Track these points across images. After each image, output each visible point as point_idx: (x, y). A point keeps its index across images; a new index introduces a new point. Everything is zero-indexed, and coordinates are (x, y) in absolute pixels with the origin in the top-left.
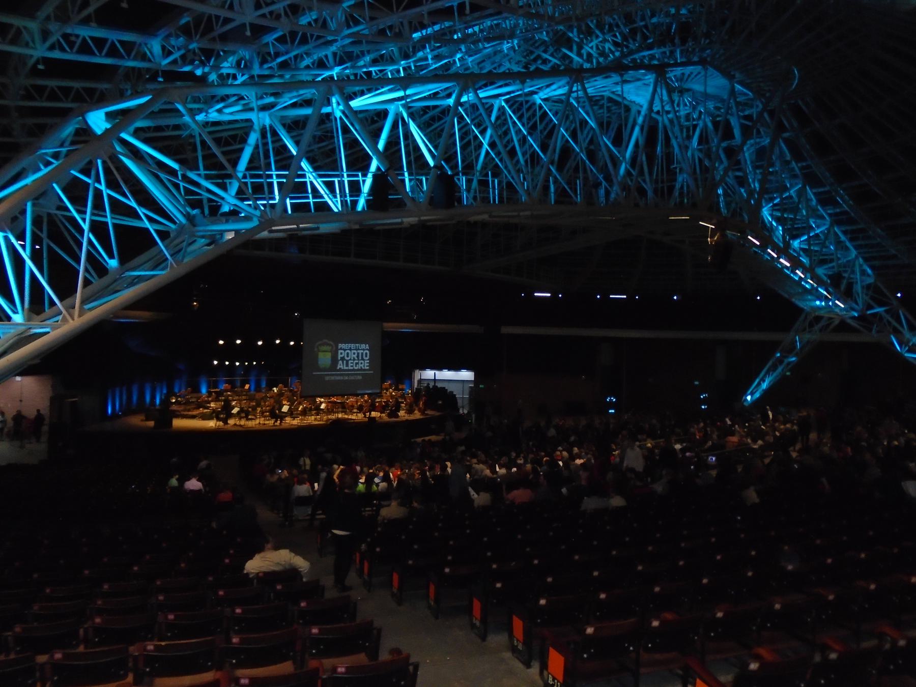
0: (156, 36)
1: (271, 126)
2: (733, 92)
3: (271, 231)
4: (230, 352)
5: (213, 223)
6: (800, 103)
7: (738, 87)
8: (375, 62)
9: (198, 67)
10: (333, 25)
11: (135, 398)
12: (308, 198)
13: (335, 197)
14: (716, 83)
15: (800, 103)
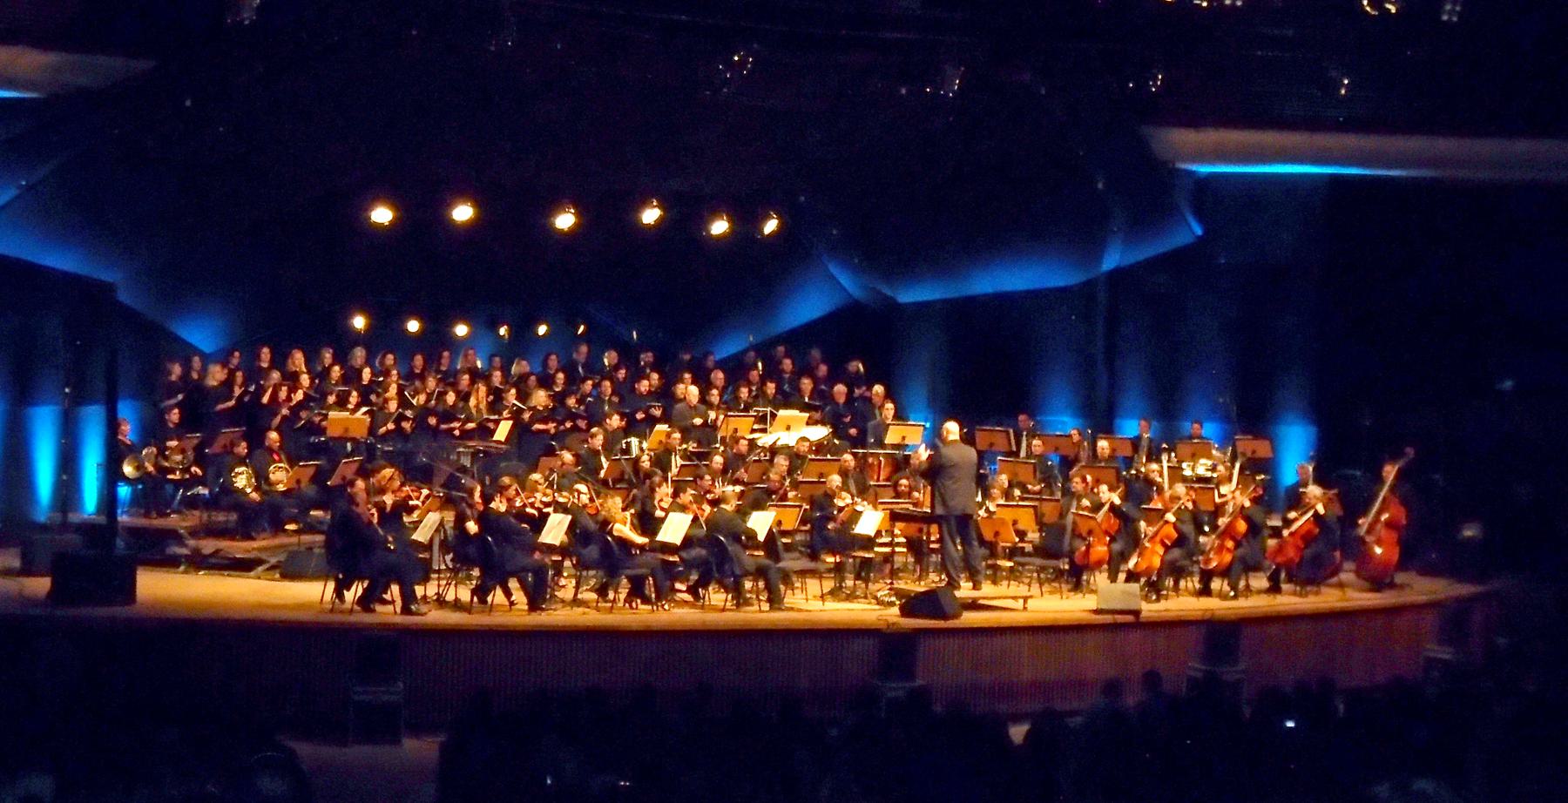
4: (428, 276)
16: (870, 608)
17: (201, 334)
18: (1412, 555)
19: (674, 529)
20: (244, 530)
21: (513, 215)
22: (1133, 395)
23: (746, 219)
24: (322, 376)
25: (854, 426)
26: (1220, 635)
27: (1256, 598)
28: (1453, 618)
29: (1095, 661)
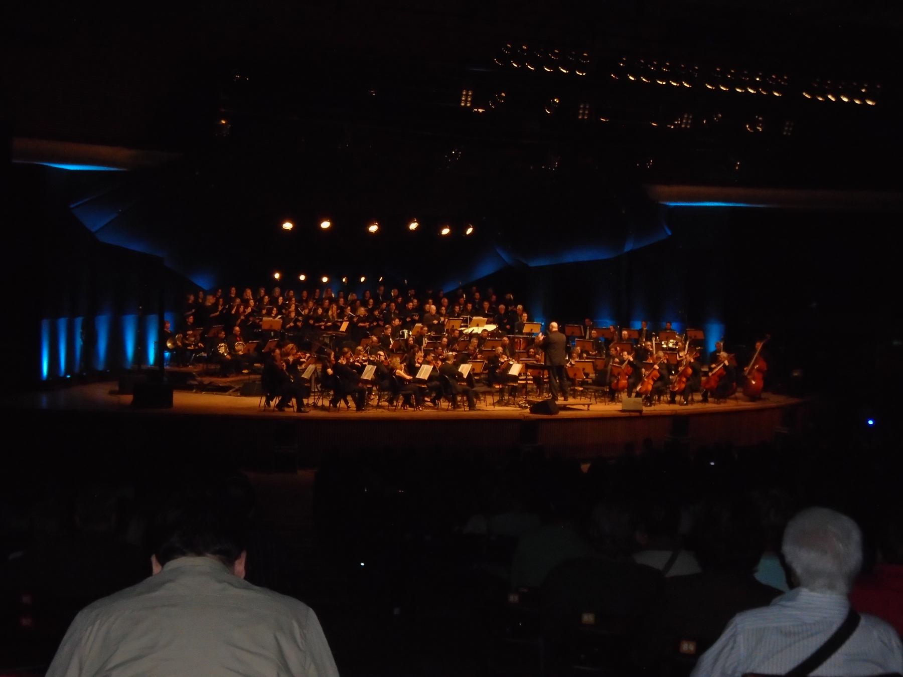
4: (307, 251)
21: (349, 226)
26: (677, 420)
27: (696, 405)
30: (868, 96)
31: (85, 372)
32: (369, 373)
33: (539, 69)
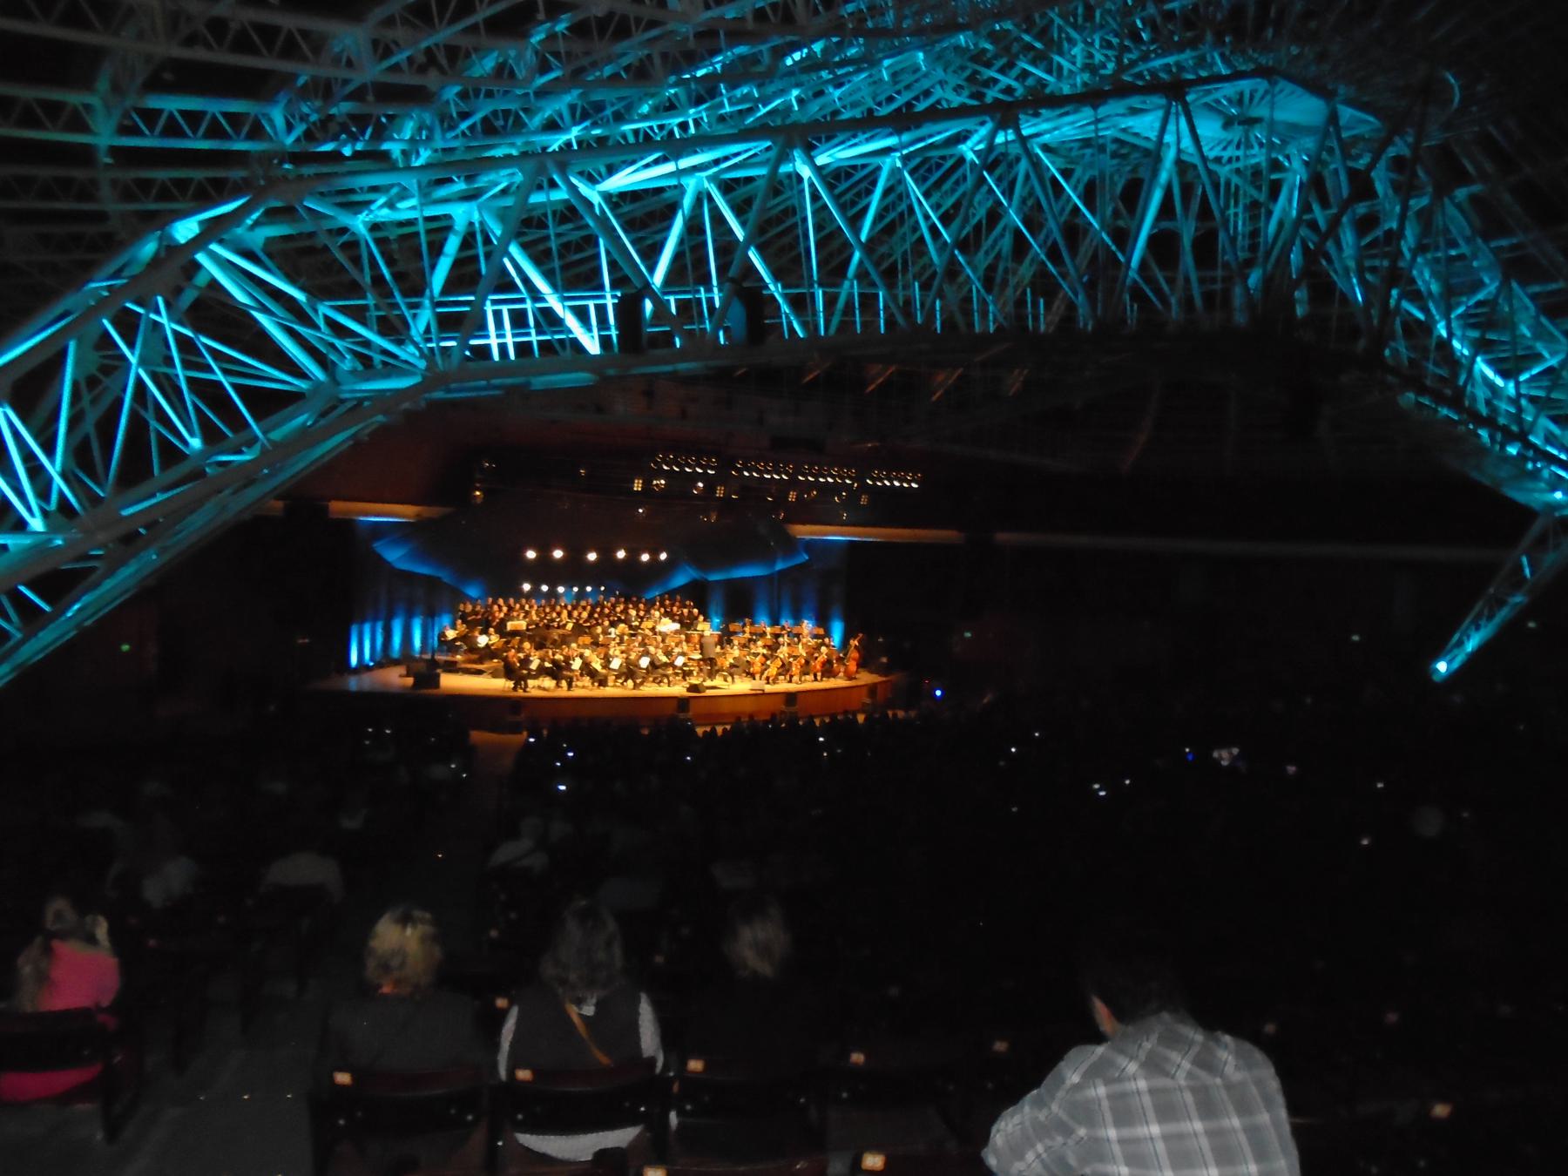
0: (277, 102)
1: (481, 223)
2: (1333, 118)
3: (449, 391)
4: (545, 571)
5: (367, 379)
6: (1491, 129)
7: (1346, 113)
8: (657, 111)
9: (344, 144)
10: (521, 73)
11: (397, 640)
12: (528, 334)
13: (590, 330)
14: (1299, 108)
15: (1491, 129)
16: (678, 689)
17: (473, 591)
18: (863, 664)
19: (616, 664)
20: (480, 661)
21: (575, 555)
22: (786, 612)
23: (654, 554)
24: (511, 609)
25: (687, 624)
26: (790, 697)
27: (809, 684)
28: (872, 689)
29: (748, 707)
30: (913, 480)
31: (385, 660)
32: (577, 664)
33: (606, 554)
